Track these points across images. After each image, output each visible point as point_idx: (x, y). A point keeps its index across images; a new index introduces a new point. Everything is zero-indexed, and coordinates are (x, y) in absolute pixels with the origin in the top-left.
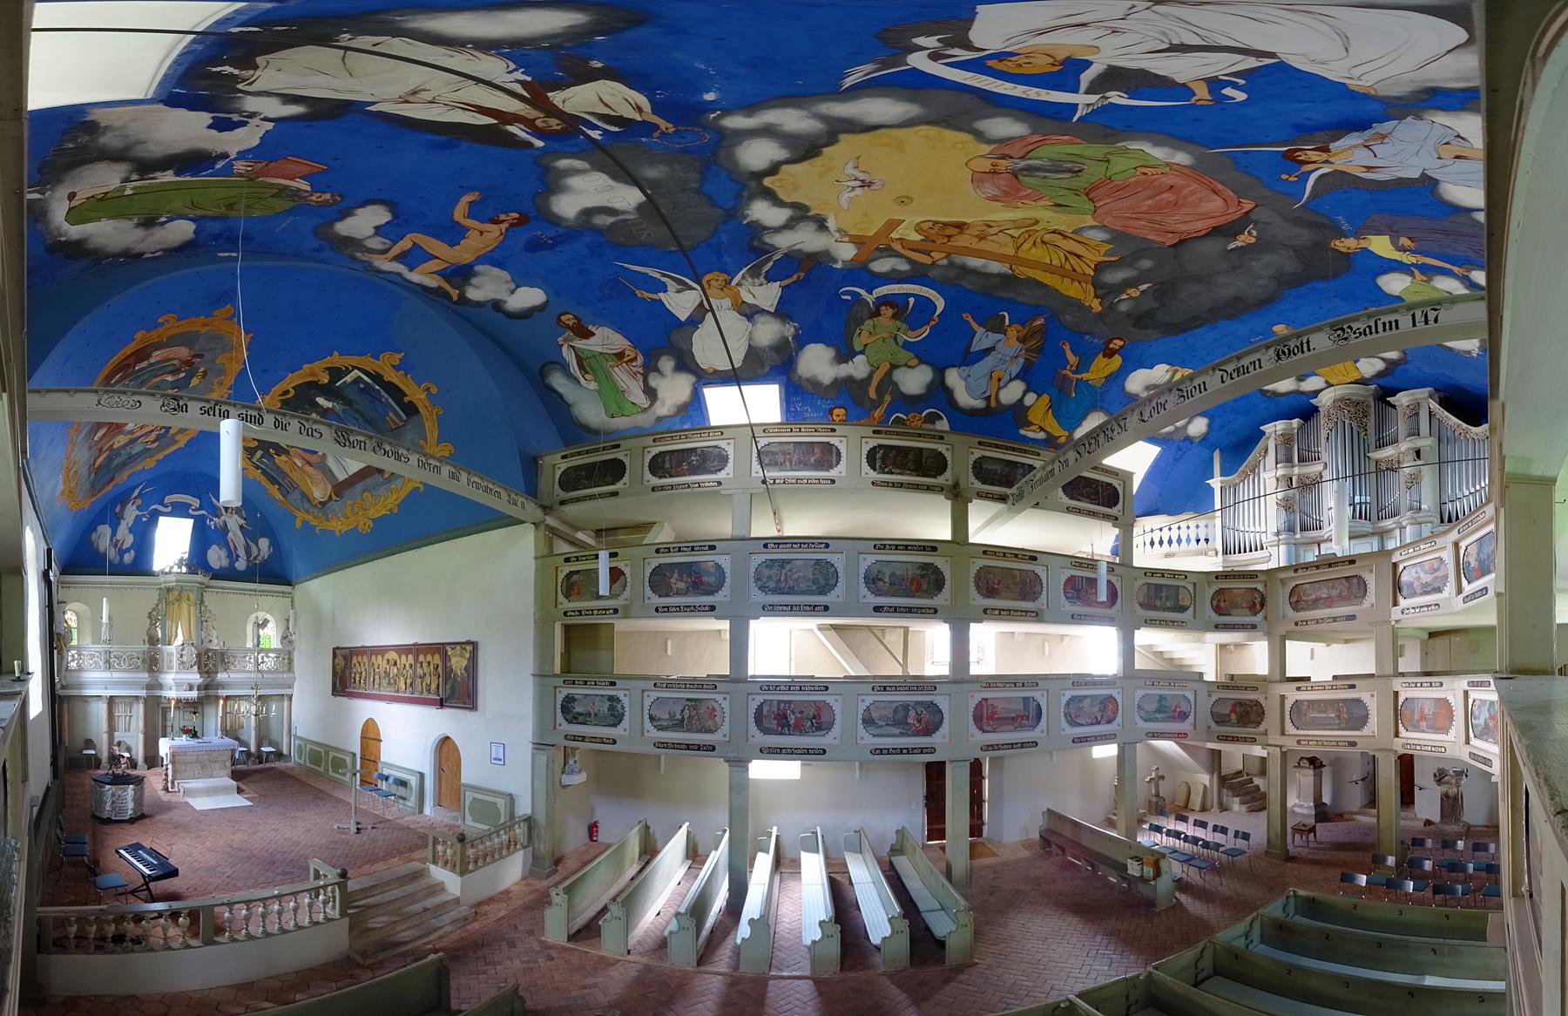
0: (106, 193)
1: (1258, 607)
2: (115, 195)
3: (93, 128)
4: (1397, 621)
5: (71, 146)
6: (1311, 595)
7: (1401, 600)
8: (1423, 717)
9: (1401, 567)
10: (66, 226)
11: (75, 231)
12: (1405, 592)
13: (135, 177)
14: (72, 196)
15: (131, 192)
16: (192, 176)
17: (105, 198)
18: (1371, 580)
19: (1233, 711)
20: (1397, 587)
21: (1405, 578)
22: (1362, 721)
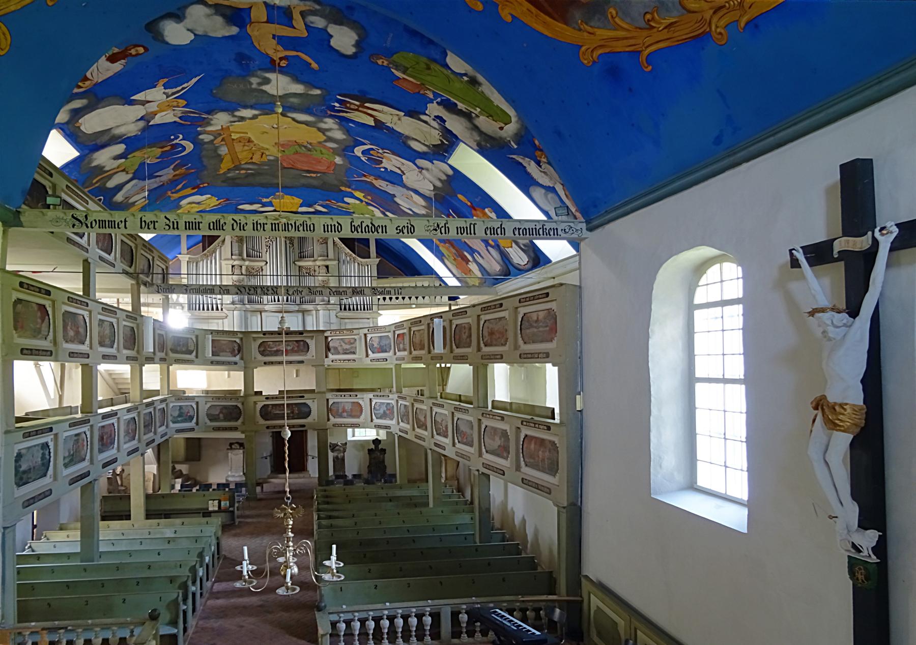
0: (488, 117)
1: (236, 352)
2: (484, 113)
3: (479, 145)
4: (328, 365)
5: (488, 145)
6: (273, 348)
7: (330, 355)
8: (344, 411)
9: (330, 339)
10: (514, 119)
11: (511, 112)
12: (332, 350)
13: (474, 115)
14: (501, 128)
15: (477, 108)
16: (450, 100)
17: (489, 116)
18: (312, 343)
19: (221, 412)
20: (328, 348)
21: (331, 345)
22: (308, 414)
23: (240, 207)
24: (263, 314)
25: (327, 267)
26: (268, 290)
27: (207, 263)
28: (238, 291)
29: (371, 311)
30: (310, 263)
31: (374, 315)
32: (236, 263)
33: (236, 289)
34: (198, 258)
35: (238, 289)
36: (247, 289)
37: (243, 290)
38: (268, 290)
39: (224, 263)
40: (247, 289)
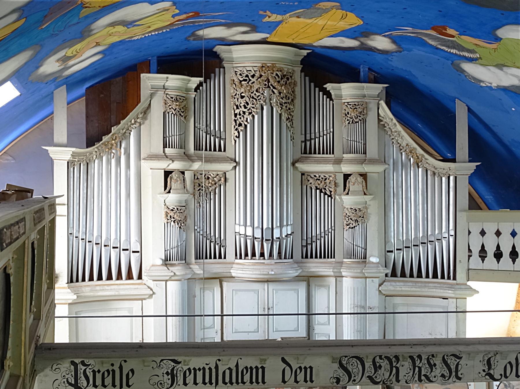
23: (194, 14)
24: (225, 284)
25: (364, 176)
26: (432, 366)
27: (109, 162)
28: (341, 372)
29: (451, 281)
30: (329, 168)
31: (459, 293)
32: (176, 166)
33: (336, 365)
34: (91, 153)
35: (341, 365)
36: (368, 364)
37: (355, 367)
38: (432, 366)
39: (146, 165)
40: (368, 364)
